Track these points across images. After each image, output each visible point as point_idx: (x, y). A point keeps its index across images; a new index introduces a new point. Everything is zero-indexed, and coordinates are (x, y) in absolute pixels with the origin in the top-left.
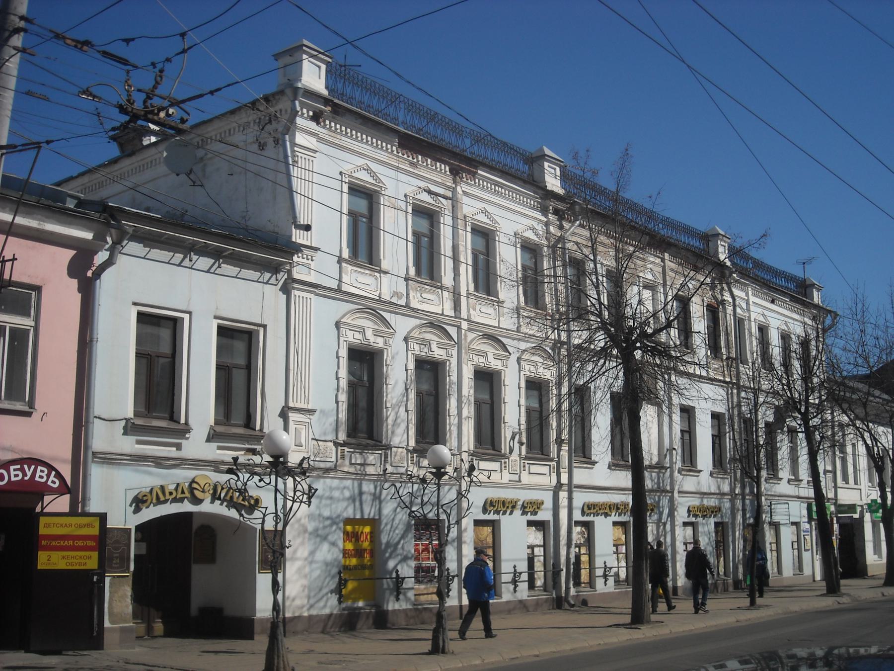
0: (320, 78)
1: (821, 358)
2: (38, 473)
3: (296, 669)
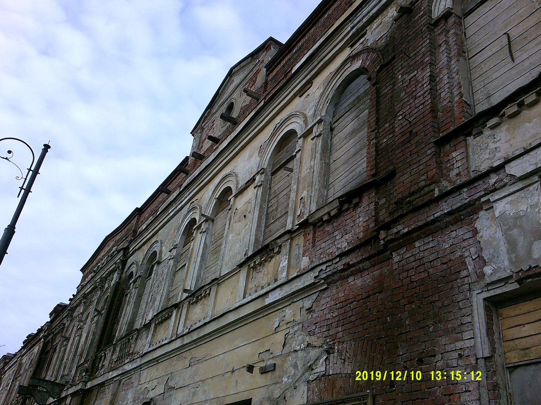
0: (18, 197)
2: (380, 376)
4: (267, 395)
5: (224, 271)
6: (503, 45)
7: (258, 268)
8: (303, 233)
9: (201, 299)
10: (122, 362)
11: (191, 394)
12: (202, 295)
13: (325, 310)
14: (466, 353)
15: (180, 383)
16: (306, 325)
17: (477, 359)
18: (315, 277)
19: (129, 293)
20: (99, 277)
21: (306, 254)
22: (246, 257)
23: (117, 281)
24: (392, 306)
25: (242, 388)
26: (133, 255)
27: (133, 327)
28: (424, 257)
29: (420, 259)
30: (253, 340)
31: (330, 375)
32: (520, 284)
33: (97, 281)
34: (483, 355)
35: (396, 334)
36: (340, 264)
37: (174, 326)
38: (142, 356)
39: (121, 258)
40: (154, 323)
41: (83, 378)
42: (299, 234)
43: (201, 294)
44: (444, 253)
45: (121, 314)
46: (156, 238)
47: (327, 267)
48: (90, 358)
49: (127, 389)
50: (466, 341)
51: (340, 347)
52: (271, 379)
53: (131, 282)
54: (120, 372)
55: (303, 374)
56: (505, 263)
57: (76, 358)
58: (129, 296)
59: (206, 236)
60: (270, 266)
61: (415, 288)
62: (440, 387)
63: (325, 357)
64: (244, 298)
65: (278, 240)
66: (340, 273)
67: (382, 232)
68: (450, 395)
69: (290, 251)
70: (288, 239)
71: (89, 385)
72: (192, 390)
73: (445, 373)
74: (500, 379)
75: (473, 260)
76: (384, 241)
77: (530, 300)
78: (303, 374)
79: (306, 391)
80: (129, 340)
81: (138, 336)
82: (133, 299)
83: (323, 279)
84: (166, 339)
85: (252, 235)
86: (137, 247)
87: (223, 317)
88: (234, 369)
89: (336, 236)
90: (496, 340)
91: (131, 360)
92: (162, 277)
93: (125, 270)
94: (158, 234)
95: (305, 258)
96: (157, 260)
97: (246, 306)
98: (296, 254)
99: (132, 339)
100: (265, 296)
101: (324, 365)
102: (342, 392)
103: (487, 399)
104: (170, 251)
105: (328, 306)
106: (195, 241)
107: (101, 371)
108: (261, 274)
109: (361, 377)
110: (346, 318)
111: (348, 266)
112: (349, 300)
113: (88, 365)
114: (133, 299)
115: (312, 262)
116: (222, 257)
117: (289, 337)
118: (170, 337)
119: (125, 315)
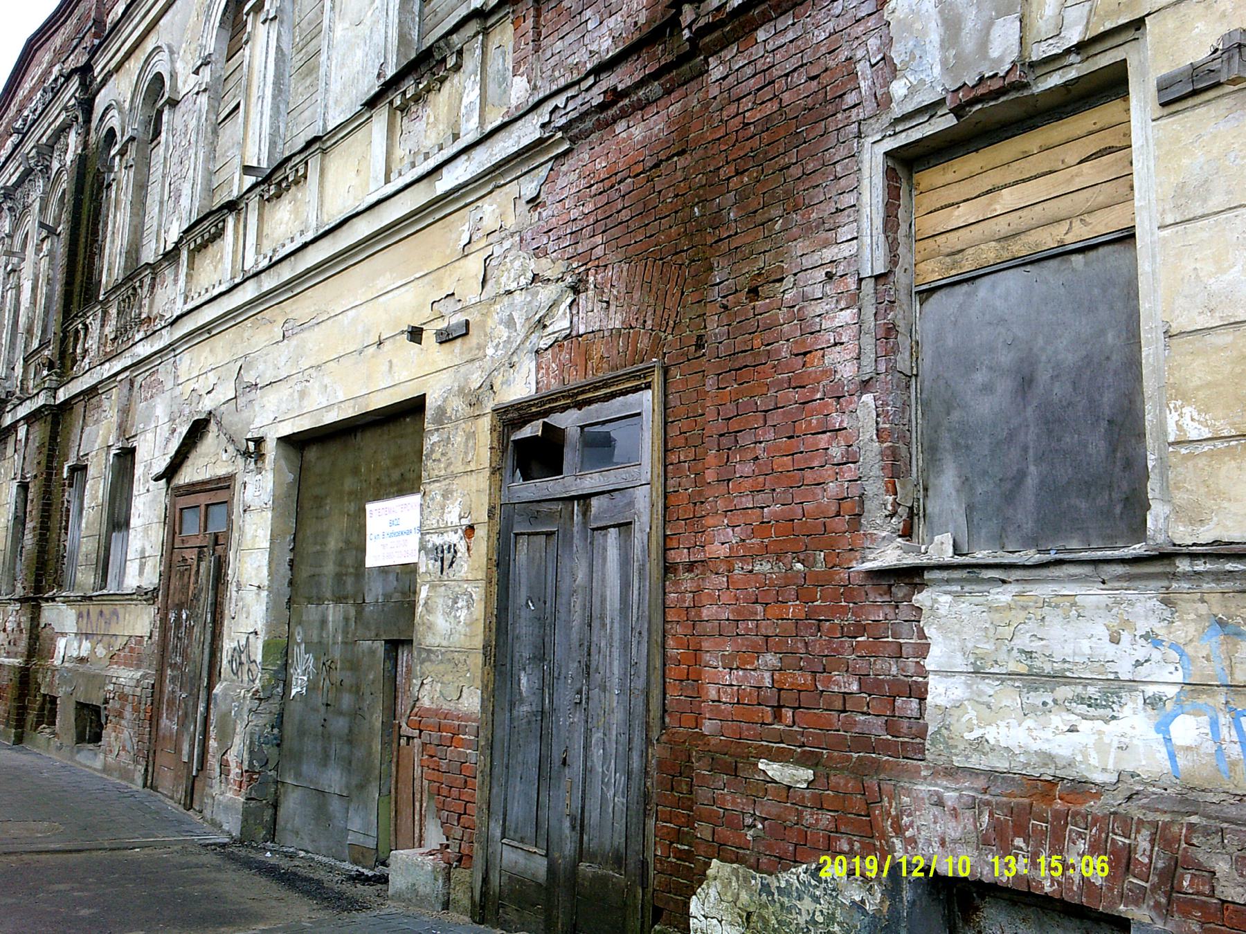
0: (1153, 120)
4: (456, 384)
5: (334, 118)
7: (414, 109)
8: (511, 16)
9: (288, 188)
10: (129, 339)
11: (296, 395)
12: (290, 180)
13: (567, 201)
14: (841, 270)
15: (268, 376)
16: (528, 236)
17: (860, 280)
18: (543, 126)
19: (114, 180)
20: (32, 144)
21: (522, 70)
22: (382, 80)
23: (79, 151)
24: (704, 182)
25: (403, 375)
26: (104, 85)
27: (137, 259)
28: (773, 66)
29: (764, 71)
30: (418, 276)
31: (581, 336)
32: (958, 117)
33: (31, 155)
34: (872, 271)
35: (710, 240)
36: (595, 90)
37: (235, 252)
38: (172, 324)
39: (77, 95)
40: (186, 248)
41: (44, 382)
42: (501, 18)
43: (287, 178)
44: (814, 53)
45: (105, 233)
46: (154, 40)
47: (568, 100)
48: (50, 336)
49: (152, 397)
50: (843, 246)
51: (599, 277)
52: (462, 353)
53: (113, 152)
54: (126, 361)
55: (527, 337)
56: (934, 70)
57: (18, 340)
58: (114, 187)
59: (279, 30)
60: (441, 101)
61: (752, 137)
62: (788, 340)
63: (569, 300)
64: (387, 181)
65: (454, 36)
66: (596, 112)
67: (687, 8)
68: (805, 354)
69: (483, 62)
70: (478, 33)
71: (62, 395)
72: (298, 388)
74: (900, 316)
75: (872, 66)
76: (691, 32)
77: (977, 151)
78: (527, 337)
79: (533, 370)
80: (134, 289)
81: (154, 279)
82: (126, 194)
83: (560, 129)
84: (220, 284)
85: (390, 25)
86: (112, 64)
87: (345, 227)
88: (382, 338)
89: (586, 21)
90: (901, 239)
91: (148, 333)
92: (185, 137)
93: (94, 124)
94: (158, 27)
95: (517, 79)
96: (166, 96)
97: (393, 199)
98: (499, 71)
99: (141, 287)
100: (434, 175)
101: (568, 315)
102: (605, 365)
103: (873, 356)
104: (196, 72)
105: (572, 191)
106: (253, 45)
107: (83, 364)
108: (422, 122)
110: (611, 216)
111: (615, 95)
112: (616, 174)
113: (50, 353)
114: (126, 194)
115: (535, 88)
116: (324, 84)
117: (493, 263)
118: (229, 277)
119: (113, 233)
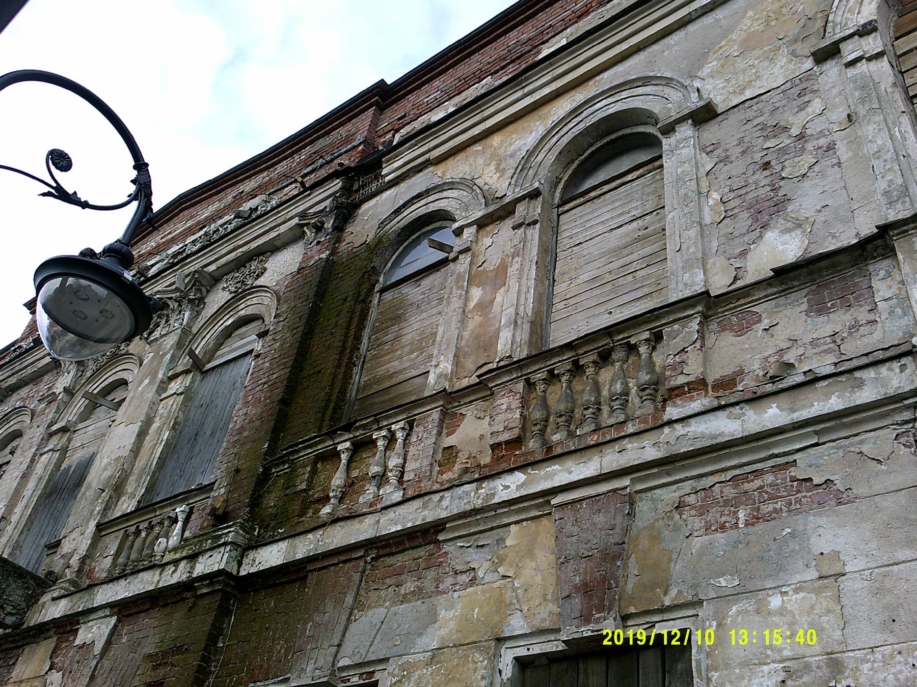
1: (793, 152)
3: (385, 679)
6: (833, 448)
73: (755, 633)
109: (612, 640)
